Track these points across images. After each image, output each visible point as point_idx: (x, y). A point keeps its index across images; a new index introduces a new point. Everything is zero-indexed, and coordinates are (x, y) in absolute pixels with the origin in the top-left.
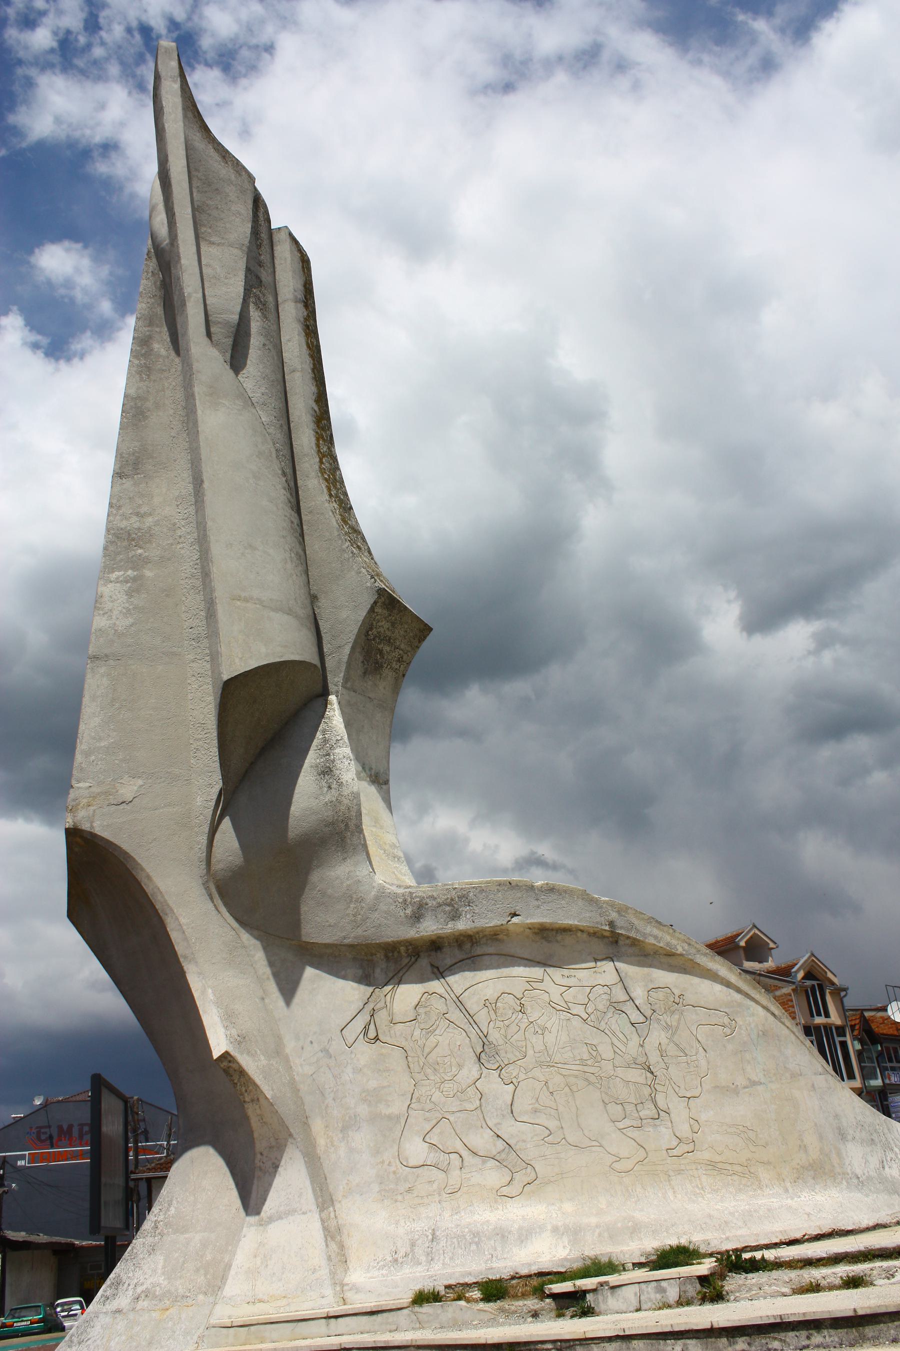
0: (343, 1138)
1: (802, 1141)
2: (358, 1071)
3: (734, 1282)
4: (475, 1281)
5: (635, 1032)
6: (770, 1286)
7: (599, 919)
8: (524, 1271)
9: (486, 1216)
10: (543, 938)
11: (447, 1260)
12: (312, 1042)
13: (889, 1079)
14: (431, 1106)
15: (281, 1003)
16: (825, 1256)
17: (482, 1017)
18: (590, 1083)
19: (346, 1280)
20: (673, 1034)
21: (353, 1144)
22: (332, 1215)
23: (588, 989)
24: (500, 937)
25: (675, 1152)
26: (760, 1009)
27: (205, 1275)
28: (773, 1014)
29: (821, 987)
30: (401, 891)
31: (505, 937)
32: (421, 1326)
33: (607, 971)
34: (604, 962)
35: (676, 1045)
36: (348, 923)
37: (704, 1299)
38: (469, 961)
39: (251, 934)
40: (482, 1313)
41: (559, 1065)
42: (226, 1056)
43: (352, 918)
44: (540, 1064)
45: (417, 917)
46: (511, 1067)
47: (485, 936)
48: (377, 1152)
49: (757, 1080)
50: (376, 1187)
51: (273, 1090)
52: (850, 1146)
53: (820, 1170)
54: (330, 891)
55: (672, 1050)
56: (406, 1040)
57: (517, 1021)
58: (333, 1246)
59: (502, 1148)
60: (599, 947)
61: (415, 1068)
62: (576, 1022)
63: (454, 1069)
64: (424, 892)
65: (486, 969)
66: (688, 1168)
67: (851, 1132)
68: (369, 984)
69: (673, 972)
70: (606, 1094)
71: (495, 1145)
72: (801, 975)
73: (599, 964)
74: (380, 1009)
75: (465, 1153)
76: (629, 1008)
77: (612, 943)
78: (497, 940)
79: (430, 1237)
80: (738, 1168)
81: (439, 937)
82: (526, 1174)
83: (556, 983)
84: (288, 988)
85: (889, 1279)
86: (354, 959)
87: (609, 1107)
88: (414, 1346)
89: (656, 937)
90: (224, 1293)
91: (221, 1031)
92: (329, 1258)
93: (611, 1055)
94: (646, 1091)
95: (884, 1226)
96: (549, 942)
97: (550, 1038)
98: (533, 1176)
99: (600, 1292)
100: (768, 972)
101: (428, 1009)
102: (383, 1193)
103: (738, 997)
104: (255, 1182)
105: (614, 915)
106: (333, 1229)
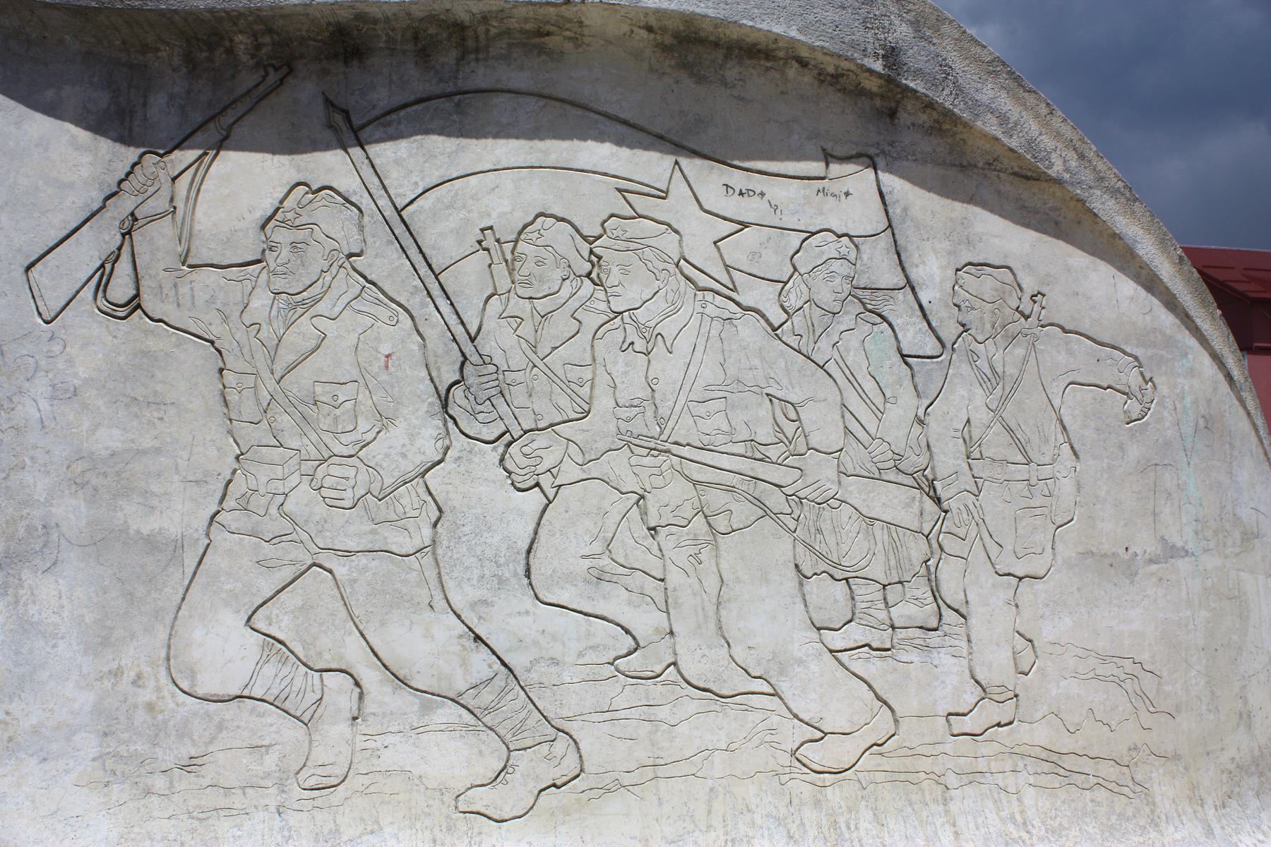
1: (1246, 702)
2: (67, 394)
5: (907, 383)
7: (859, 35)
10: (684, 65)
17: (469, 279)
18: (766, 512)
20: (1004, 399)
21: (32, 610)
23: (795, 239)
24: (551, 42)
25: (967, 724)
26: (1206, 360)
28: (1229, 377)
31: (569, 46)
34: (851, 167)
35: (1010, 430)
38: (446, 105)
41: (685, 451)
44: (629, 442)
46: (541, 440)
47: (507, 32)
48: (102, 640)
49: (1180, 544)
50: (89, 745)
56: (226, 319)
57: (573, 304)
59: (487, 673)
60: (841, 119)
62: (750, 329)
63: (363, 425)
65: (496, 136)
66: (994, 766)
68: (125, 139)
69: (1027, 225)
70: (809, 546)
71: (464, 663)
73: (835, 169)
74: (153, 218)
75: (370, 675)
76: (900, 309)
77: (879, 113)
78: (542, 50)
80: (1108, 770)
83: (701, 203)
87: (812, 586)
89: (1003, 119)
94: (916, 549)
96: (700, 80)
97: (668, 369)
101: (301, 235)
102: (110, 764)
103: (1167, 320)
105: (901, 32)
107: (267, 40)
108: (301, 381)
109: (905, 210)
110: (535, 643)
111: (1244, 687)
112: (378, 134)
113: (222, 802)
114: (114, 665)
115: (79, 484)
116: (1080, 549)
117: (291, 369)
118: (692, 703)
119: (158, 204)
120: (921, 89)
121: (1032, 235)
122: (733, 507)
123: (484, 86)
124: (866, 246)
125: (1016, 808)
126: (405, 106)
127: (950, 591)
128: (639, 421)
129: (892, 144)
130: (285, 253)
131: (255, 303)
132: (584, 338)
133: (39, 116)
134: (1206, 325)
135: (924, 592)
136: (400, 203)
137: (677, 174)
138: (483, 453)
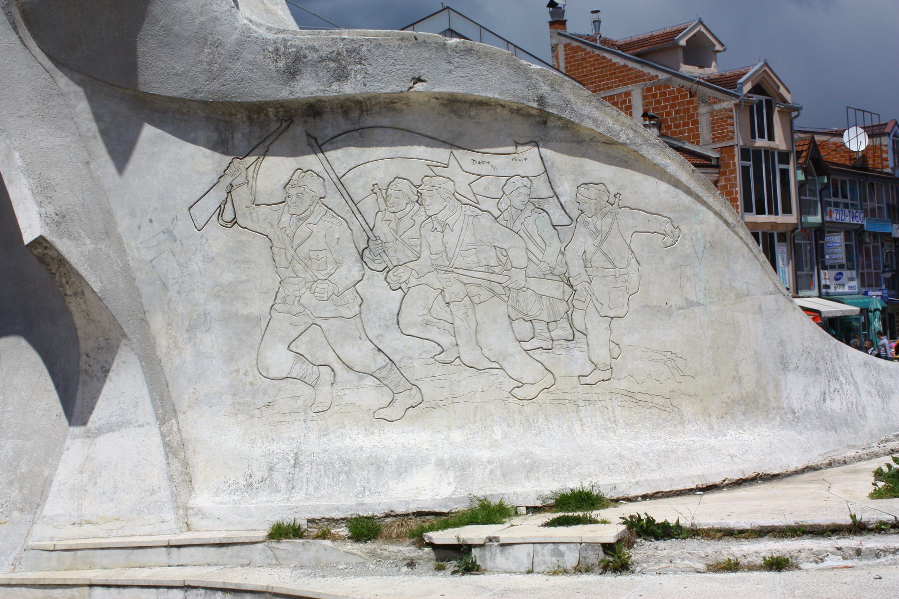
0: (190, 339)
1: (738, 372)
2: (209, 260)
3: (643, 551)
4: (343, 516)
5: (556, 237)
6: (683, 559)
7: (526, 93)
8: (401, 510)
9: (358, 441)
10: (453, 111)
11: (311, 490)
12: (151, 221)
13: (831, 216)
14: (300, 309)
15: (111, 169)
16: (749, 527)
17: (369, 206)
18: (495, 294)
19: (191, 503)
20: (602, 241)
21: (201, 347)
22: (175, 428)
23: (504, 180)
24: (398, 106)
25: (588, 380)
26: (711, 215)
27: (21, 489)
28: (726, 222)
29: (769, 103)
30: (271, 36)
31: (404, 107)
32: (278, 563)
33: (530, 159)
34: (527, 147)
35: (605, 254)
36: (201, 72)
37: (606, 568)
38: (355, 134)
39: (71, 78)
40: (349, 555)
41: (460, 271)
42: (40, 241)
43: (205, 66)
44: (436, 268)
45: (292, 73)
46: (401, 270)
47: (379, 103)
49: (695, 300)
51: (101, 282)
52: (791, 376)
53: (753, 405)
54: (176, 28)
55: (598, 260)
56: (272, 226)
57: (412, 213)
58: (176, 464)
59: (384, 364)
60: (522, 127)
61: (282, 261)
62: (485, 220)
63: (330, 267)
64: (302, 40)
65: (377, 146)
67: (795, 360)
69: (611, 164)
71: (374, 360)
72: (748, 87)
73: (520, 149)
75: (338, 367)
76: (552, 206)
77: (539, 123)
78: (394, 109)
79: (292, 462)
81: (319, 101)
82: (410, 396)
83: (461, 168)
84: (121, 151)
85: (817, 562)
86: (208, 118)
87: (515, 324)
88: (270, 593)
89: (595, 121)
90: (45, 513)
91: (34, 209)
92: (171, 478)
93: (523, 262)
94: (562, 307)
95: (814, 469)
96: (460, 117)
97: (451, 238)
98: (418, 399)
99: (488, 548)
100: (708, 81)
101: (301, 190)
102: (237, 407)
104: (80, 386)
106: (175, 445)
107: (281, 110)
108: (304, 250)
109: (552, 163)
110: (402, 351)
111: (737, 365)
112: (329, 148)
113: (282, 419)
114: (236, 368)
115: (217, 296)
116: (642, 304)
117: (299, 245)
118: (468, 372)
119: (241, 179)
120: (555, 112)
121: (614, 168)
122: (481, 293)
123: (371, 125)
124: (535, 181)
125: (611, 414)
126: (339, 135)
127: (578, 322)
128: (440, 260)
129: (545, 136)
130: (294, 198)
131: (283, 219)
132: (417, 227)
133: (189, 145)
134: (710, 199)
136: (340, 176)
137: (452, 157)
138: (378, 276)
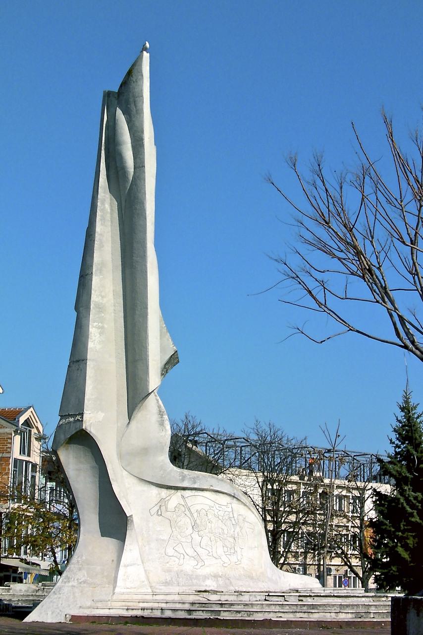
17: (195, 515)
44: (209, 532)
46: (201, 532)
55: (240, 534)
61: (173, 527)
62: (220, 521)
75: (185, 554)
76: (233, 519)
93: (226, 533)
97: (213, 525)
108: (179, 524)
135: (311, 563)
